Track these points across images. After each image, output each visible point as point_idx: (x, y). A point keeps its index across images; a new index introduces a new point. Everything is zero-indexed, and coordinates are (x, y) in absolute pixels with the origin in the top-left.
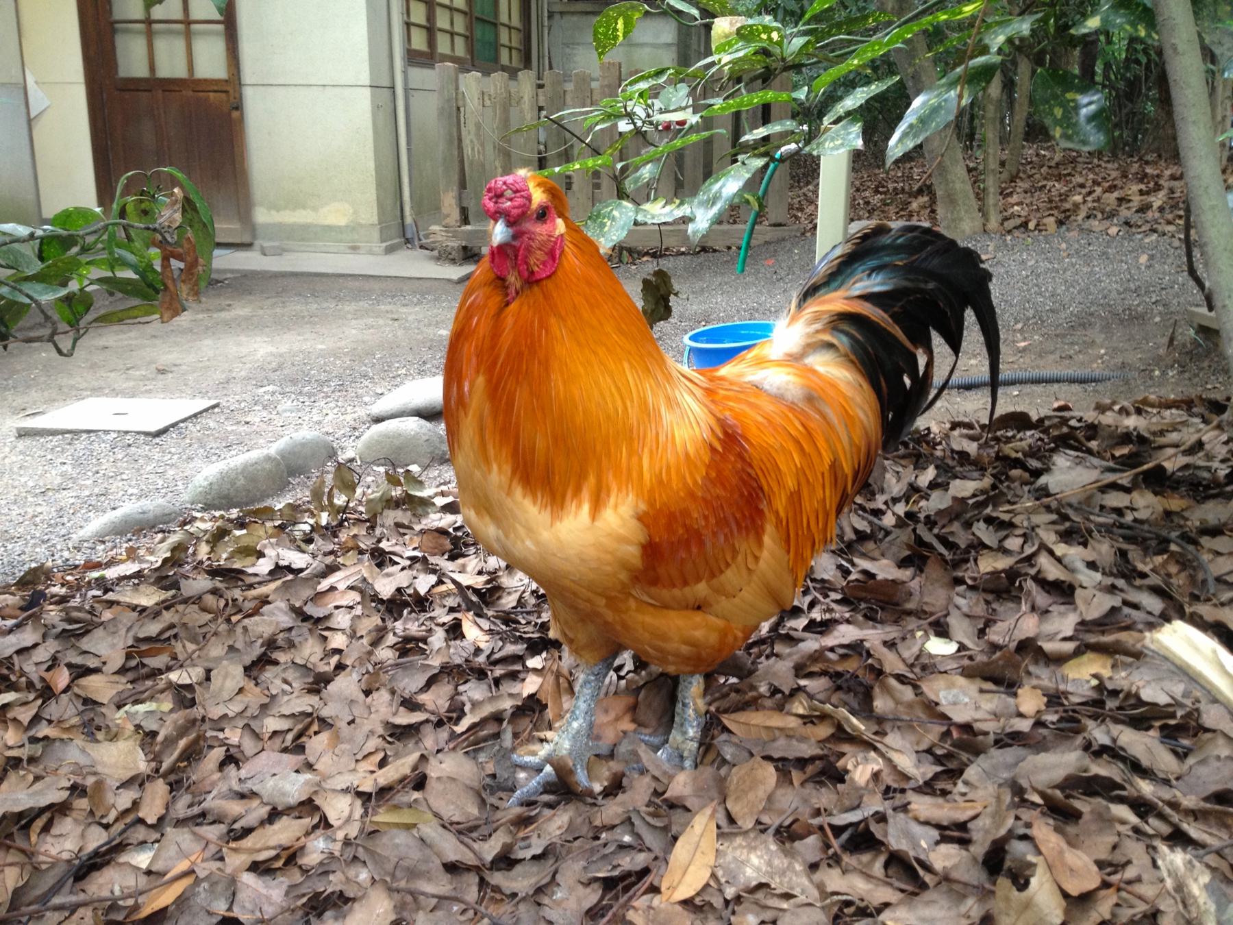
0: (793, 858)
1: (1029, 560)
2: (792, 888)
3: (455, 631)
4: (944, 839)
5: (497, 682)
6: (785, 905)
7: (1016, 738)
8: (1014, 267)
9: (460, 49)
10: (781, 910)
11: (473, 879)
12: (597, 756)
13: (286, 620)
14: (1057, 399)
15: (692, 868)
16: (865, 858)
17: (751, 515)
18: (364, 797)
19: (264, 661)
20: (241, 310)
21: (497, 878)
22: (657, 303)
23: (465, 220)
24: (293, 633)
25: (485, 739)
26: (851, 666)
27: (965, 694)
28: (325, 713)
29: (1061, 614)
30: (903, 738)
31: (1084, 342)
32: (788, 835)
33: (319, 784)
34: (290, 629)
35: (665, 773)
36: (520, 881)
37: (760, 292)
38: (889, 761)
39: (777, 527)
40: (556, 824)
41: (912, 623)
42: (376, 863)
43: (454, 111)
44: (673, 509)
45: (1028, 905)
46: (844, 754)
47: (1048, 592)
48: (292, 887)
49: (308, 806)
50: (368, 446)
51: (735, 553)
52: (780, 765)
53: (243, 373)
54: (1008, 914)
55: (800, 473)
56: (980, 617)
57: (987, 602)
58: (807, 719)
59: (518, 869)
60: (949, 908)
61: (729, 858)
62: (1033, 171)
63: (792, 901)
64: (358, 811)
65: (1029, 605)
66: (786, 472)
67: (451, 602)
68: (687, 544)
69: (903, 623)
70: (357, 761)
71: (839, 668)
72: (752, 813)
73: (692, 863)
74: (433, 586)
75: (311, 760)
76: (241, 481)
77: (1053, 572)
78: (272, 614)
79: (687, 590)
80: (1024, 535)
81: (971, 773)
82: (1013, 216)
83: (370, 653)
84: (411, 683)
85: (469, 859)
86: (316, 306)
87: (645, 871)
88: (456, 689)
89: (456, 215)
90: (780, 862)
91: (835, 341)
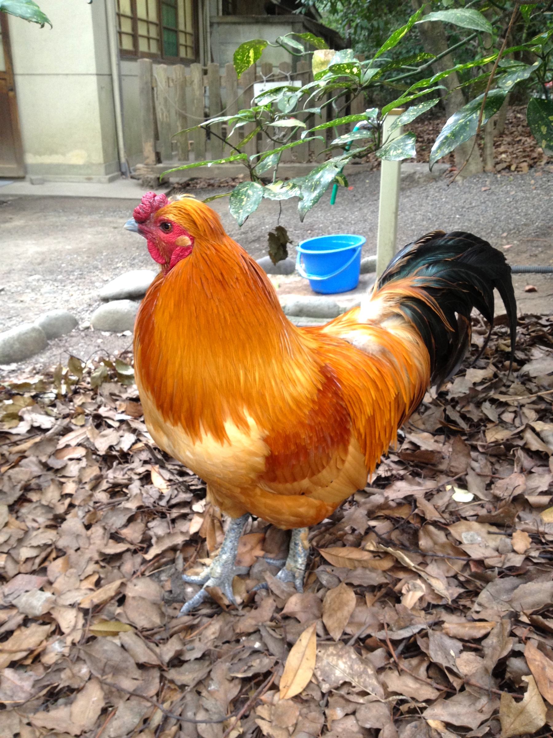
0: (367, 665)
1: (520, 435)
2: (366, 687)
3: (146, 478)
4: (466, 649)
5: (173, 521)
6: (361, 701)
7: (512, 571)
8: (502, 195)
9: (154, 49)
10: (358, 703)
11: (156, 674)
12: (239, 575)
13: (36, 470)
14: (528, 284)
15: (300, 671)
16: (414, 661)
17: (341, 434)
18: (86, 612)
19: (23, 500)
20: (18, 222)
21: (172, 674)
22: (278, 249)
23: (159, 161)
24: (42, 479)
25: (166, 564)
26: (404, 513)
27: (479, 535)
28: (61, 544)
29: (540, 475)
30: (439, 568)
31: (545, 246)
32: (364, 645)
33: (55, 602)
34: (39, 477)
35: (283, 592)
36: (186, 676)
37: (345, 210)
38: (429, 586)
39: (358, 439)
40: (212, 629)
41: (443, 479)
42: (92, 662)
43: (150, 90)
44: (288, 433)
45: (522, 712)
46: (400, 580)
47: (531, 457)
48: (37, 682)
49: (46, 619)
50: (99, 319)
51: (329, 459)
52: (358, 590)
53: (19, 266)
54: (508, 716)
55: (375, 405)
56: (487, 476)
57: (492, 464)
58: (376, 554)
59: (186, 666)
60: (470, 706)
61: (325, 662)
62: (514, 129)
63: (366, 698)
64: (81, 621)
65: (519, 468)
66: (367, 402)
67: (145, 456)
68: (297, 455)
69: (438, 479)
70: (81, 580)
71: (396, 515)
72: (340, 627)
73: (302, 666)
74: (134, 444)
75: (52, 579)
76: (17, 346)
77: (535, 445)
78: (27, 466)
79: (295, 484)
80: (515, 412)
81: (483, 596)
82: (501, 161)
83: (91, 496)
84: (117, 521)
85: (154, 660)
86: (65, 218)
87: (268, 674)
88: (146, 526)
89: (153, 157)
90: (358, 667)
91: (401, 313)
